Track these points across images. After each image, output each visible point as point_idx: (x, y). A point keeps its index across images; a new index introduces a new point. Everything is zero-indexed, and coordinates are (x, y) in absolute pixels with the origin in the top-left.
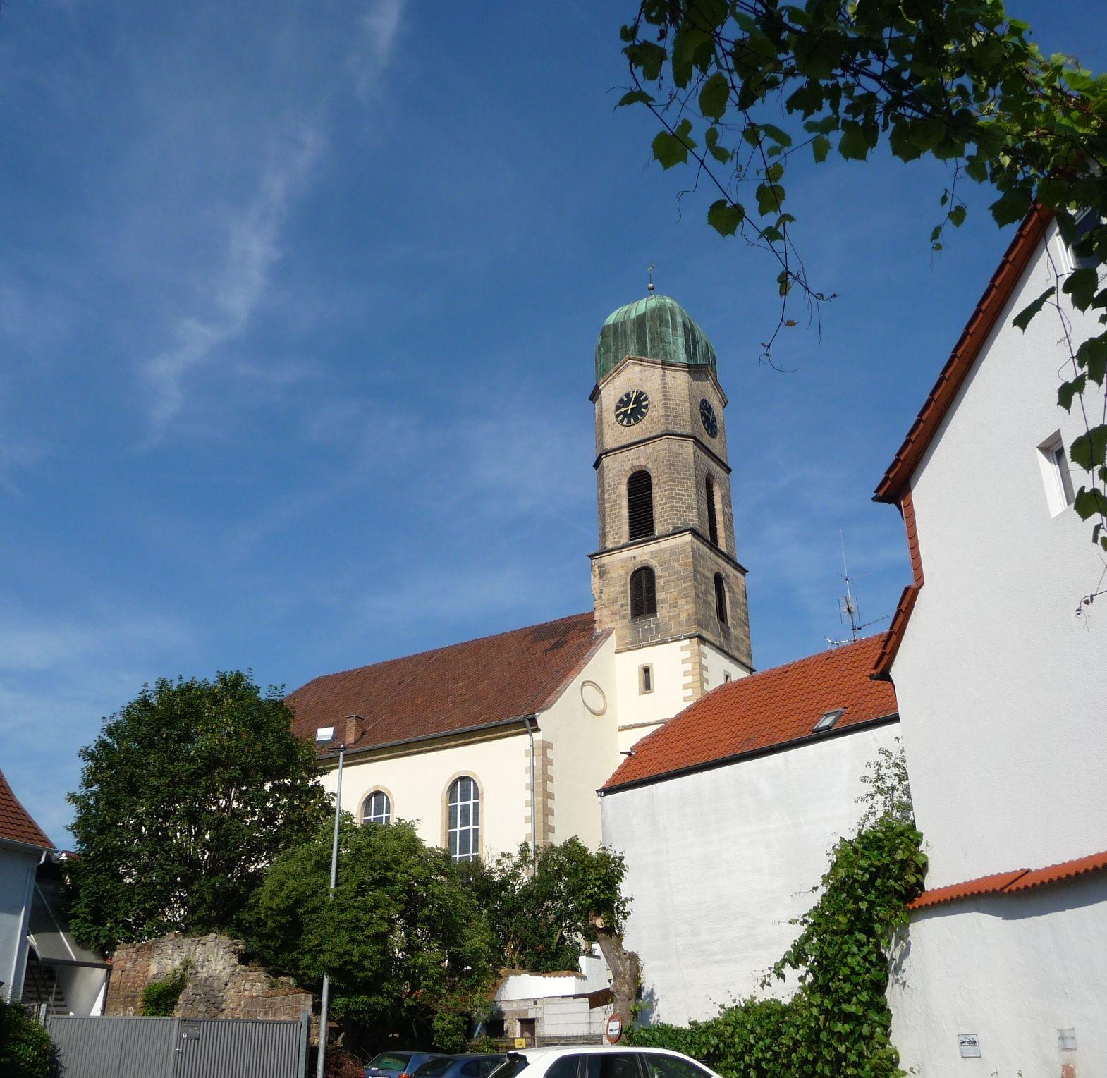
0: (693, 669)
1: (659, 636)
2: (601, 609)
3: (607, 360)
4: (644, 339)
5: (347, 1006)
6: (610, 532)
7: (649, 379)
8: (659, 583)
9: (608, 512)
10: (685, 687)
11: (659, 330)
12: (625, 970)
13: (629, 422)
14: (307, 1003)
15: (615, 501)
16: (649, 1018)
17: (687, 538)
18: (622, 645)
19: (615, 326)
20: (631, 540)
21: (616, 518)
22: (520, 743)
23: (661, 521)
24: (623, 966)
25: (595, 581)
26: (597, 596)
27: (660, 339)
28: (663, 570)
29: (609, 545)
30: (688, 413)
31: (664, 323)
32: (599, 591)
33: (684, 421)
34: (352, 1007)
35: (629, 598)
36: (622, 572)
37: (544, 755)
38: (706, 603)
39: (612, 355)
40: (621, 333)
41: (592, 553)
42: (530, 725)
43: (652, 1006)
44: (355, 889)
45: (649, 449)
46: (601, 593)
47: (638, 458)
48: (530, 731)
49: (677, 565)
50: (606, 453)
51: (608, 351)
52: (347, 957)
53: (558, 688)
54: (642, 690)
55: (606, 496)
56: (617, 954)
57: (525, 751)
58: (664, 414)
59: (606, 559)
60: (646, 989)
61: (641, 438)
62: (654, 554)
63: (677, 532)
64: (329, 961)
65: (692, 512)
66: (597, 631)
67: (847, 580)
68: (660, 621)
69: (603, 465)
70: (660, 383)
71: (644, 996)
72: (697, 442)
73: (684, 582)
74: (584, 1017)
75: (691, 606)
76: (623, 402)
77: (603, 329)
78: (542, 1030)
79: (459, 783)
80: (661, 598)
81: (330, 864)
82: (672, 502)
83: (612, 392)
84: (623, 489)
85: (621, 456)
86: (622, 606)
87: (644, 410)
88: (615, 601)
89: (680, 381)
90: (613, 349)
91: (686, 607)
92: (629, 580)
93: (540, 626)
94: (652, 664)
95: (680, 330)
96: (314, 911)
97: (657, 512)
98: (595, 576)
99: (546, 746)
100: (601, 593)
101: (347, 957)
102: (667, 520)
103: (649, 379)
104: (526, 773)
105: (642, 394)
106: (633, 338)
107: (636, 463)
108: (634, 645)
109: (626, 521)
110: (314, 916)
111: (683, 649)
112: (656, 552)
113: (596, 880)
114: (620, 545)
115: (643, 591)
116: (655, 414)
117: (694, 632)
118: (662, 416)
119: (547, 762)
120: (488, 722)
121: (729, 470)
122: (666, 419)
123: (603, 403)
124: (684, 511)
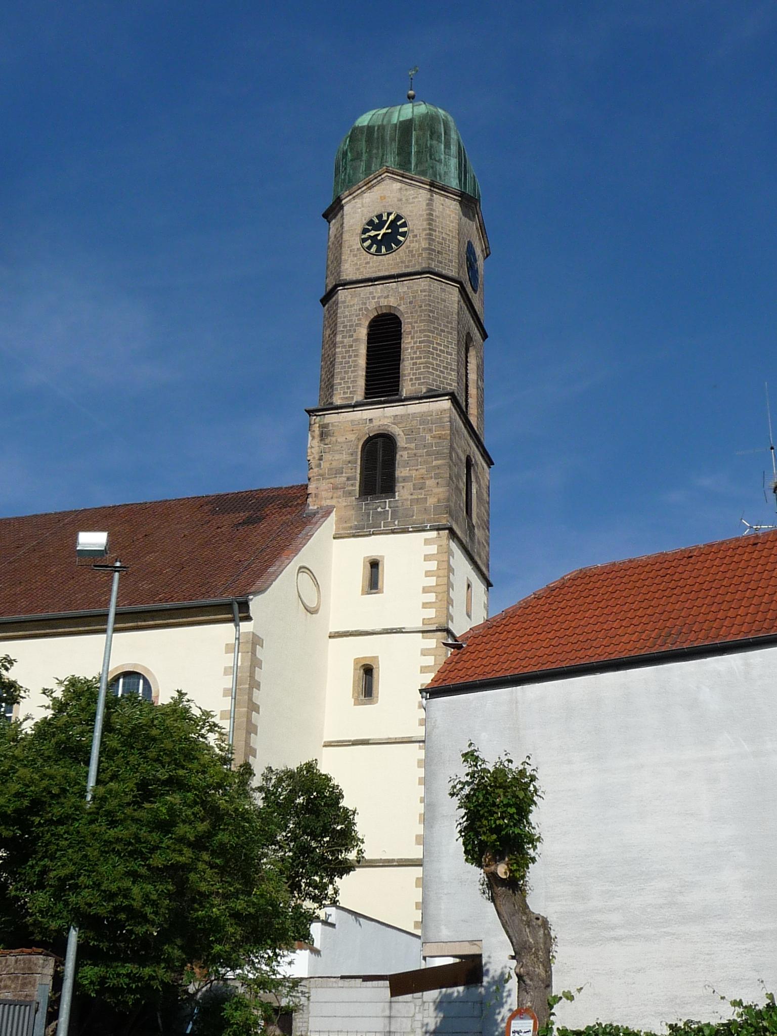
0: (438, 569)
1: (396, 523)
2: (318, 480)
3: (355, 169)
4: (409, 150)
5: (103, 980)
6: (340, 384)
7: (411, 200)
8: (402, 456)
9: (339, 359)
10: (426, 590)
11: (429, 143)
12: (537, 942)
13: (379, 250)
14: (45, 971)
15: (351, 346)
16: (495, 1014)
17: (445, 404)
18: (344, 529)
19: (370, 129)
20: (366, 398)
21: (350, 367)
22: (224, 632)
23: (411, 380)
24: (535, 937)
25: (314, 445)
26: (314, 463)
27: (428, 154)
28: (409, 441)
29: (337, 401)
30: (456, 251)
31: (435, 136)
32: (317, 457)
33: (451, 261)
34: (110, 983)
35: (359, 471)
36: (352, 437)
37: (254, 652)
38: (458, 488)
39: (363, 164)
40: (378, 138)
41: (312, 408)
42: (237, 610)
43: (502, 998)
44: (132, 790)
45: (403, 287)
46: (320, 459)
47: (387, 297)
48: (238, 619)
49: (428, 437)
50: (345, 284)
51: (357, 157)
52: (119, 900)
53: (271, 570)
54: (367, 588)
55: (339, 338)
56: (524, 918)
57: (227, 645)
58: (427, 246)
59: (331, 418)
60: (491, 973)
61: (393, 272)
62: (397, 420)
63: (432, 395)
64: (86, 904)
65: (451, 375)
66: (311, 508)
67: (772, 448)
68: (400, 504)
69: (337, 299)
70: (424, 207)
71: (488, 982)
72: (463, 291)
73: (436, 459)
74: (381, 1008)
75: (441, 490)
76: (375, 223)
77: (353, 131)
78: (305, 1024)
79: (121, 681)
80: (403, 475)
81: (88, 753)
82: (429, 358)
83: (358, 210)
84: (363, 333)
85: (365, 291)
86: (348, 479)
87: (401, 238)
88: (339, 472)
89: (449, 210)
90: (365, 157)
91: (436, 490)
92: (360, 447)
93: (219, 497)
94: (383, 557)
95: (454, 149)
96: (60, 822)
97: (407, 367)
98: (313, 437)
99: (256, 641)
100: (320, 459)
101: (119, 900)
102: (419, 379)
103: (411, 200)
104: (226, 673)
105: (399, 217)
106: (395, 146)
107: (384, 302)
108: (359, 532)
109: (362, 373)
110: (61, 829)
111: (427, 542)
112: (402, 416)
113: (508, 805)
114: (353, 403)
115: (378, 465)
116: (415, 245)
117: (444, 521)
118: (424, 249)
119: (255, 663)
120: (172, 601)
121: (485, 336)
122: (429, 254)
123: (345, 221)
124: (441, 371)
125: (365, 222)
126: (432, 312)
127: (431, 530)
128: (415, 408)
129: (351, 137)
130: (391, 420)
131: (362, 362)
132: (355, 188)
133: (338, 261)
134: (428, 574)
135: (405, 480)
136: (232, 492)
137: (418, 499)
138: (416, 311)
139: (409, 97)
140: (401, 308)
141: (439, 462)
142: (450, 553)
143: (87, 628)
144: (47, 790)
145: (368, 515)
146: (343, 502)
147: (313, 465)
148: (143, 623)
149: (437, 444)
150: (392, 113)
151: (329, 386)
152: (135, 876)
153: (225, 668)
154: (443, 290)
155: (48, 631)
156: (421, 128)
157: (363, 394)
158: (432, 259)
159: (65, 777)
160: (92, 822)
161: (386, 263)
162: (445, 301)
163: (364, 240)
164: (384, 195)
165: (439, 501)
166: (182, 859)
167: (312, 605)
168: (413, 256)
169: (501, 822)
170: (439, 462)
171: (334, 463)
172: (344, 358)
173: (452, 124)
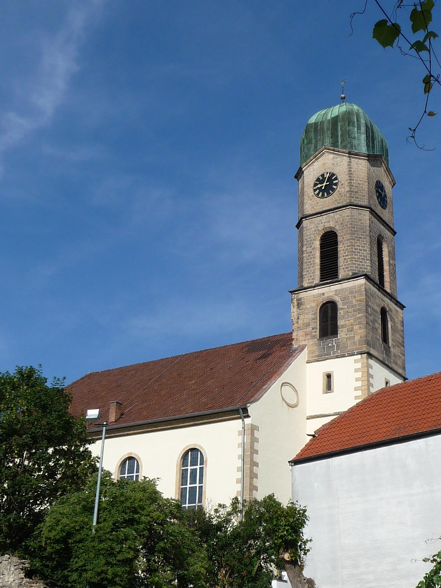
0: (362, 376)
3: (309, 149)
4: (336, 135)
6: (306, 274)
15: (311, 252)
17: (362, 281)
18: (312, 357)
19: (316, 124)
20: (321, 281)
21: (311, 265)
22: (234, 426)
23: (344, 269)
25: (294, 310)
26: (295, 321)
27: (348, 135)
28: (344, 304)
29: (305, 285)
30: (366, 190)
33: (364, 196)
35: (318, 324)
36: (314, 304)
37: (252, 434)
38: (374, 329)
39: (313, 145)
42: (244, 413)
45: (336, 215)
46: (298, 319)
47: (329, 222)
49: (354, 301)
50: (306, 217)
51: (310, 142)
53: (264, 387)
55: (304, 248)
59: (302, 295)
61: (332, 207)
63: (355, 276)
68: (340, 341)
70: (347, 167)
72: (372, 212)
73: (359, 313)
76: (320, 181)
79: (190, 453)
80: (341, 324)
83: (312, 172)
84: (317, 244)
85: (317, 220)
86: (313, 329)
88: (308, 325)
89: (361, 166)
91: (359, 331)
94: (333, 372)
95: (363, 129)
96: (80, 541)
97: (341, 261)
98: (294, 306)
99: (254, 428)
100: (298, 319)
101: (103, 575)
102: (348, 268)
104: (239, 447)
105: (333, 175)
106: (329, 132)
108: (321, 357)
109: (318, 267)
110: (80, 545)
111: (356, 361)
113: (285, 525)
114: (313, 285)
115: (329, 318)
118: (348, 192)
119: (254, 440)
123: (305, 180)
125: (315, 179)
126: (353, 227)
127: (357, 354)
128: (346, 285)
129: (306, 131)
130: (334, 293)
131: (318, 261)
132: (309, 160)
133: (302, 204)
134: (357, 380)
135: (343, 327)
136: (260, 338)
137: (350, 337)
138: (345, 228)
139: (342, 98)
140: (336, 227)
141: (360, 315)
142: (369, 366)
143: (171, 426)
144: (74, 527)
145: (324, 349)
146: (311, 342)
147: (294, 322)
148: (198, 422)
149: (359, 305)
150: (328, 113)
151: (301, 277)
152: (108, 563)
153: (238, 444)
154: (360, 214)
155: (153, 429)
156: (343, 120)
157: (319, 279)
158: (352, 197)
159: (82, 521)
160: (93, 541)
161: (328, 202)
162: (361, 220)
163: (315, 190)
164: (327, 162)
165: (361, 338)
166: (130, 556)
167: (293, 402)
168: (342, 196)
169: (282, 534)
170: (360, 315)
171: (305, 320)
172: (307, 259)
173: (361, 115)
